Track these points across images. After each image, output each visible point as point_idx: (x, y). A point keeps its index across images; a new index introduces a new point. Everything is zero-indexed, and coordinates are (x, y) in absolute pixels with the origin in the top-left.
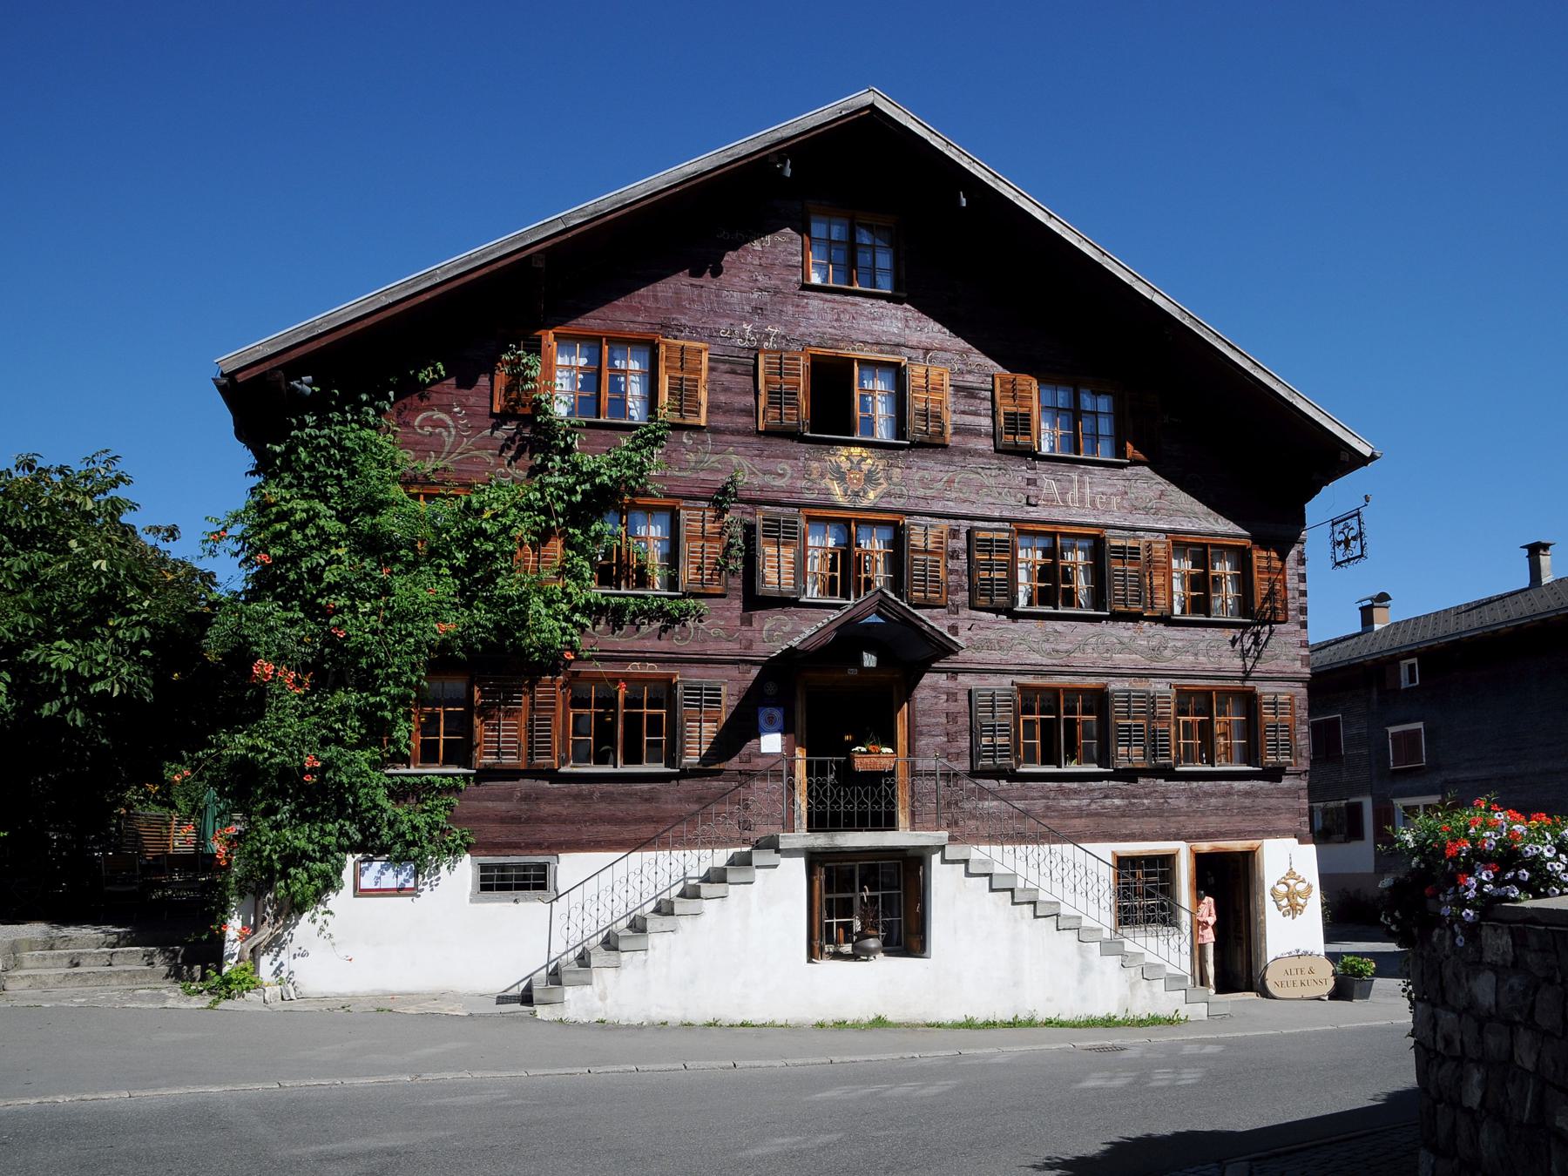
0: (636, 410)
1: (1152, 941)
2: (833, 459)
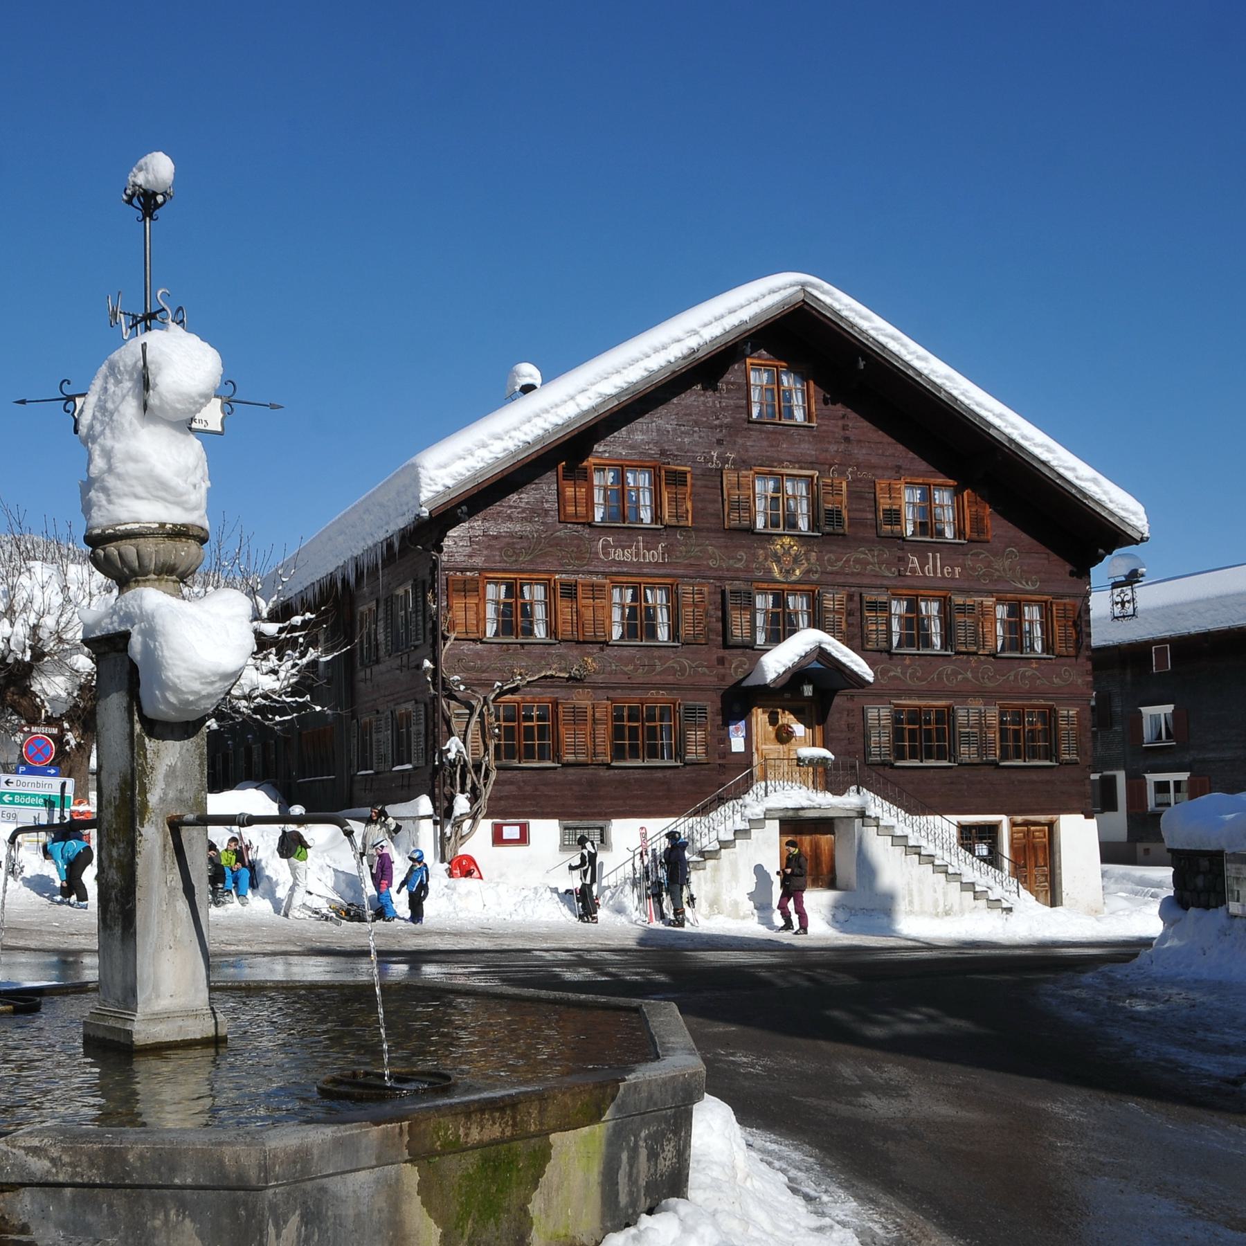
0: (646, 515)
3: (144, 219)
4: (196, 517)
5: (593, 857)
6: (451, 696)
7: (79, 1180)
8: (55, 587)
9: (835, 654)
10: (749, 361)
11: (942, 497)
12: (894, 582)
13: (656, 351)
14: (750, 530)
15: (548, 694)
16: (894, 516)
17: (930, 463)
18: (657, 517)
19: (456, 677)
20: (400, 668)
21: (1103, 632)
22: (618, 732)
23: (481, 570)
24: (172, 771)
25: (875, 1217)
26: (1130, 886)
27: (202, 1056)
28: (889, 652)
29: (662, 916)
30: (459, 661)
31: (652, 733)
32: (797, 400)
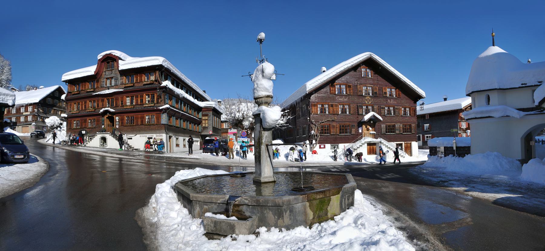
0: (345, 93)
3: (260, 44)
4: (271, 94)
5: (336, 150)
6: (312, 124)
7: (252, 205)
8: (246, 107)
9: (376, 116)
10: (362, 67)
11: (393, 90)
12: (386, 104)
13: (346, 65)
14: (362, 95)
15: (329, 123)
16: (386, 93)
17: (391, 84)
18: (346, 93)
19: (313, 121)
20: (304, 119)
21: (419, 112)
22: (340, 129)
23: (317, 102)
24: (266, 136)
25: (385, 208)
26: (423, 153)
27: (273, 184)
28: (385, 116)
29: (348, 160)
30: (314, 118)
31: (346, 129)
32: (370, 73)
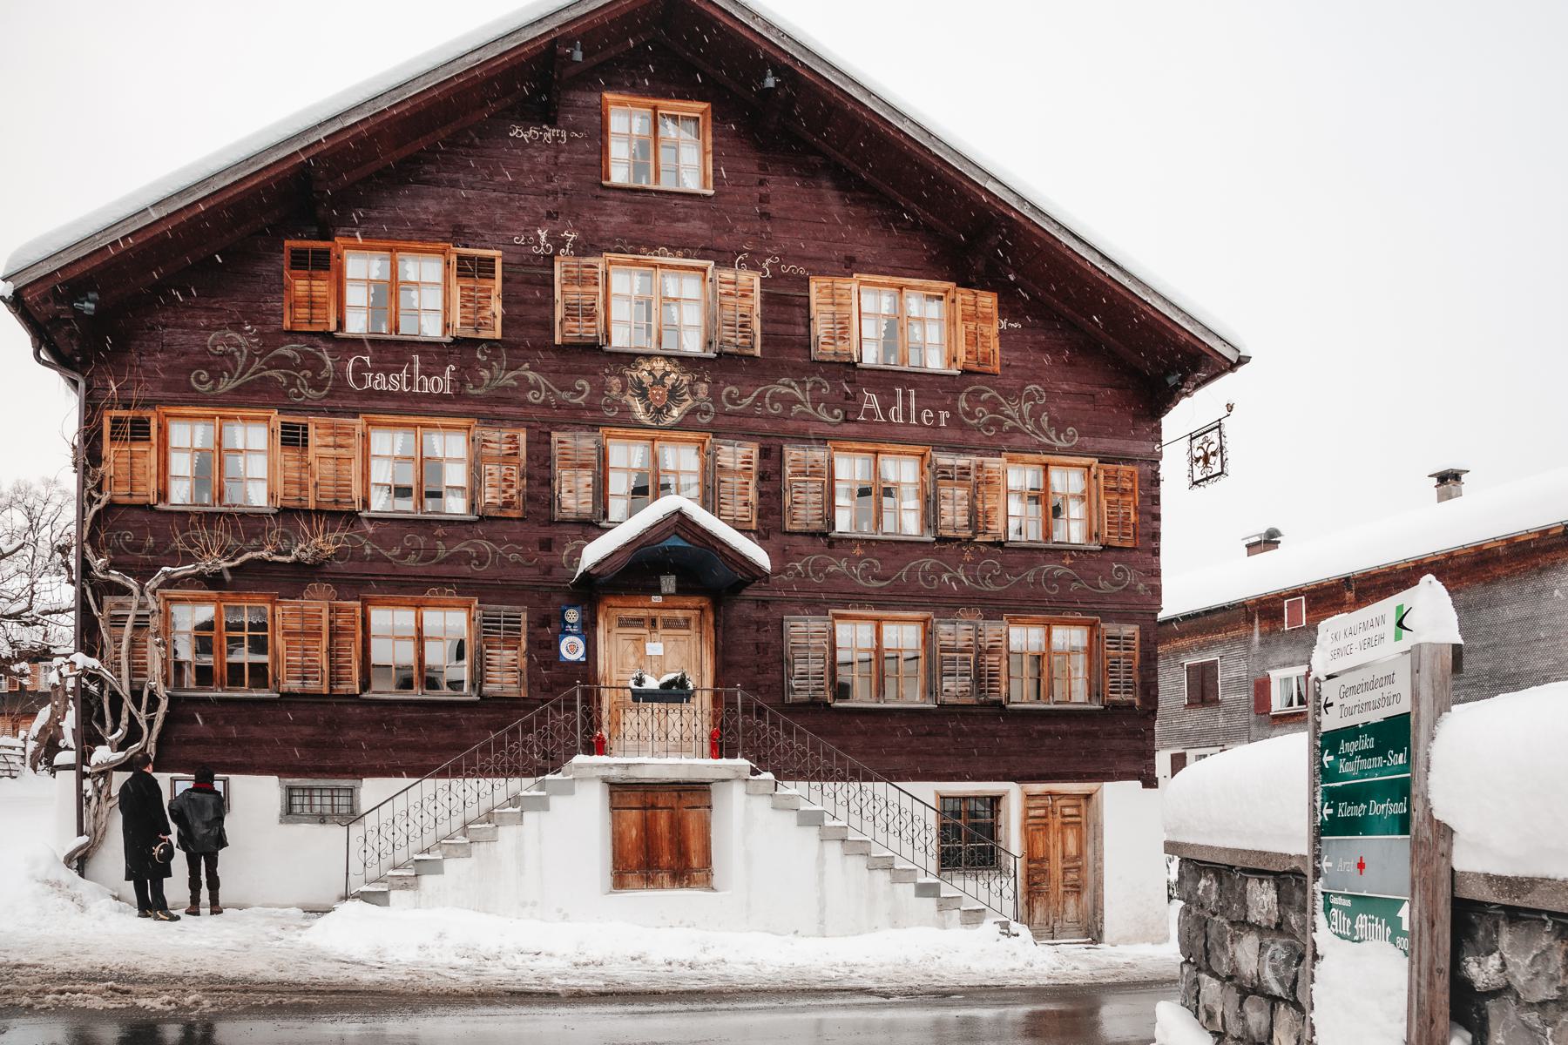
1: (971, 884)
2: (634, 374)
